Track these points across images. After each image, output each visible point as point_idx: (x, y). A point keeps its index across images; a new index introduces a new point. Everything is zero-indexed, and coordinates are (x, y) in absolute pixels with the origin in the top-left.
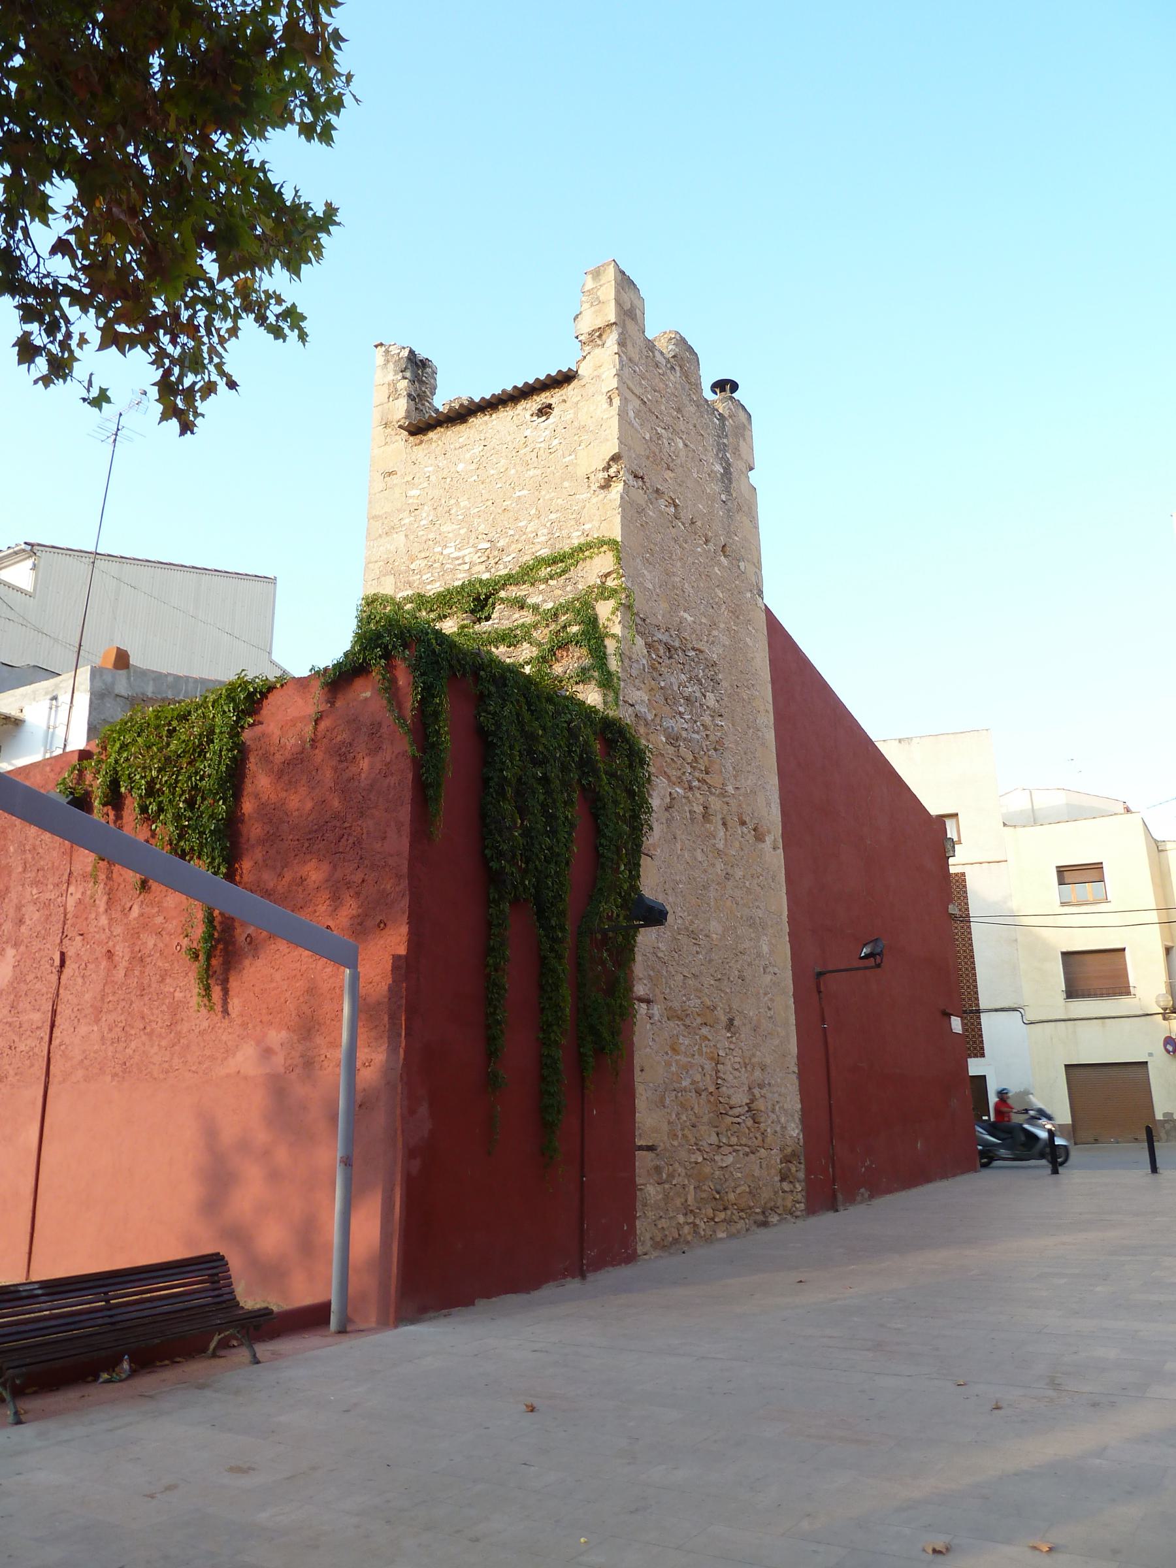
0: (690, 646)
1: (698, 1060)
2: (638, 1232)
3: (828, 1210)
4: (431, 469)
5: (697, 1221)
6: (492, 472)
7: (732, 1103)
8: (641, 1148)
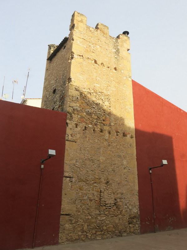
0: (98, 92)
7: (106, 203)
8: (62, 215)
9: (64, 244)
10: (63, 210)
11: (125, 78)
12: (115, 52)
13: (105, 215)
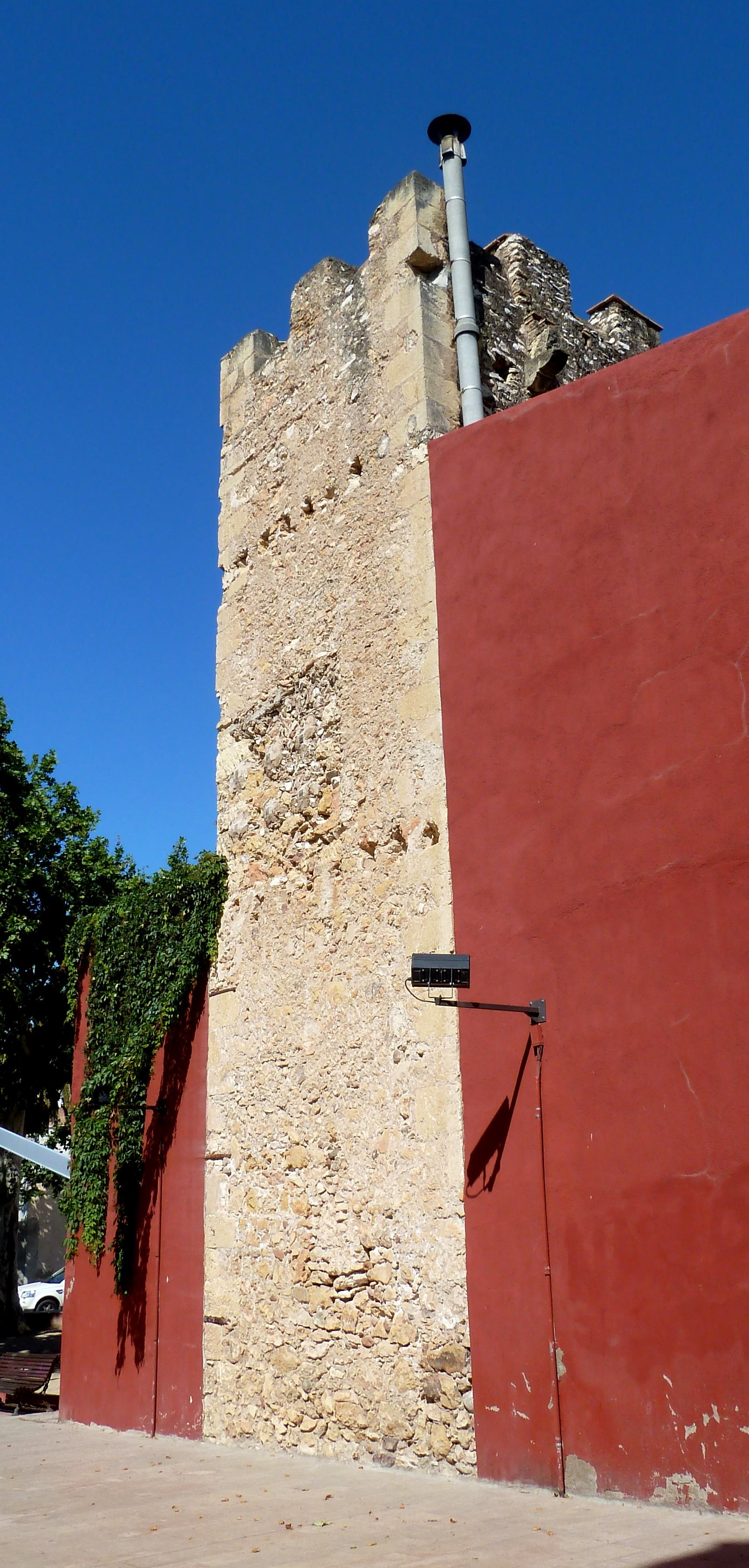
1: (282, 1215)
2: (205, 1410)
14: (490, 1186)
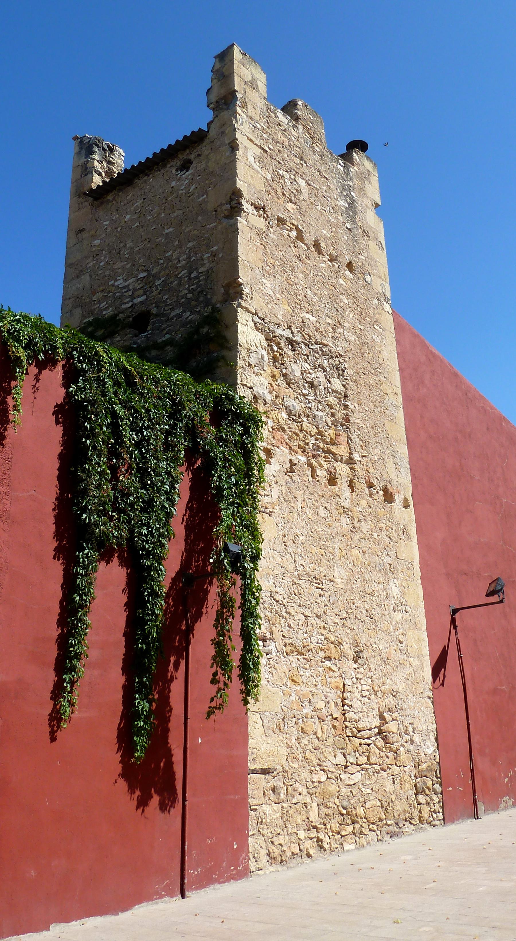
3: (469, 817)
4: (107, 223)
5: (321, 836)
6: (149, 218)
7: (361, 726)
9: (265, 873)
10: (252, 753)
11: (376, 301)
12: (346, 208)
13: (359, 768)
14: (443, 684)
